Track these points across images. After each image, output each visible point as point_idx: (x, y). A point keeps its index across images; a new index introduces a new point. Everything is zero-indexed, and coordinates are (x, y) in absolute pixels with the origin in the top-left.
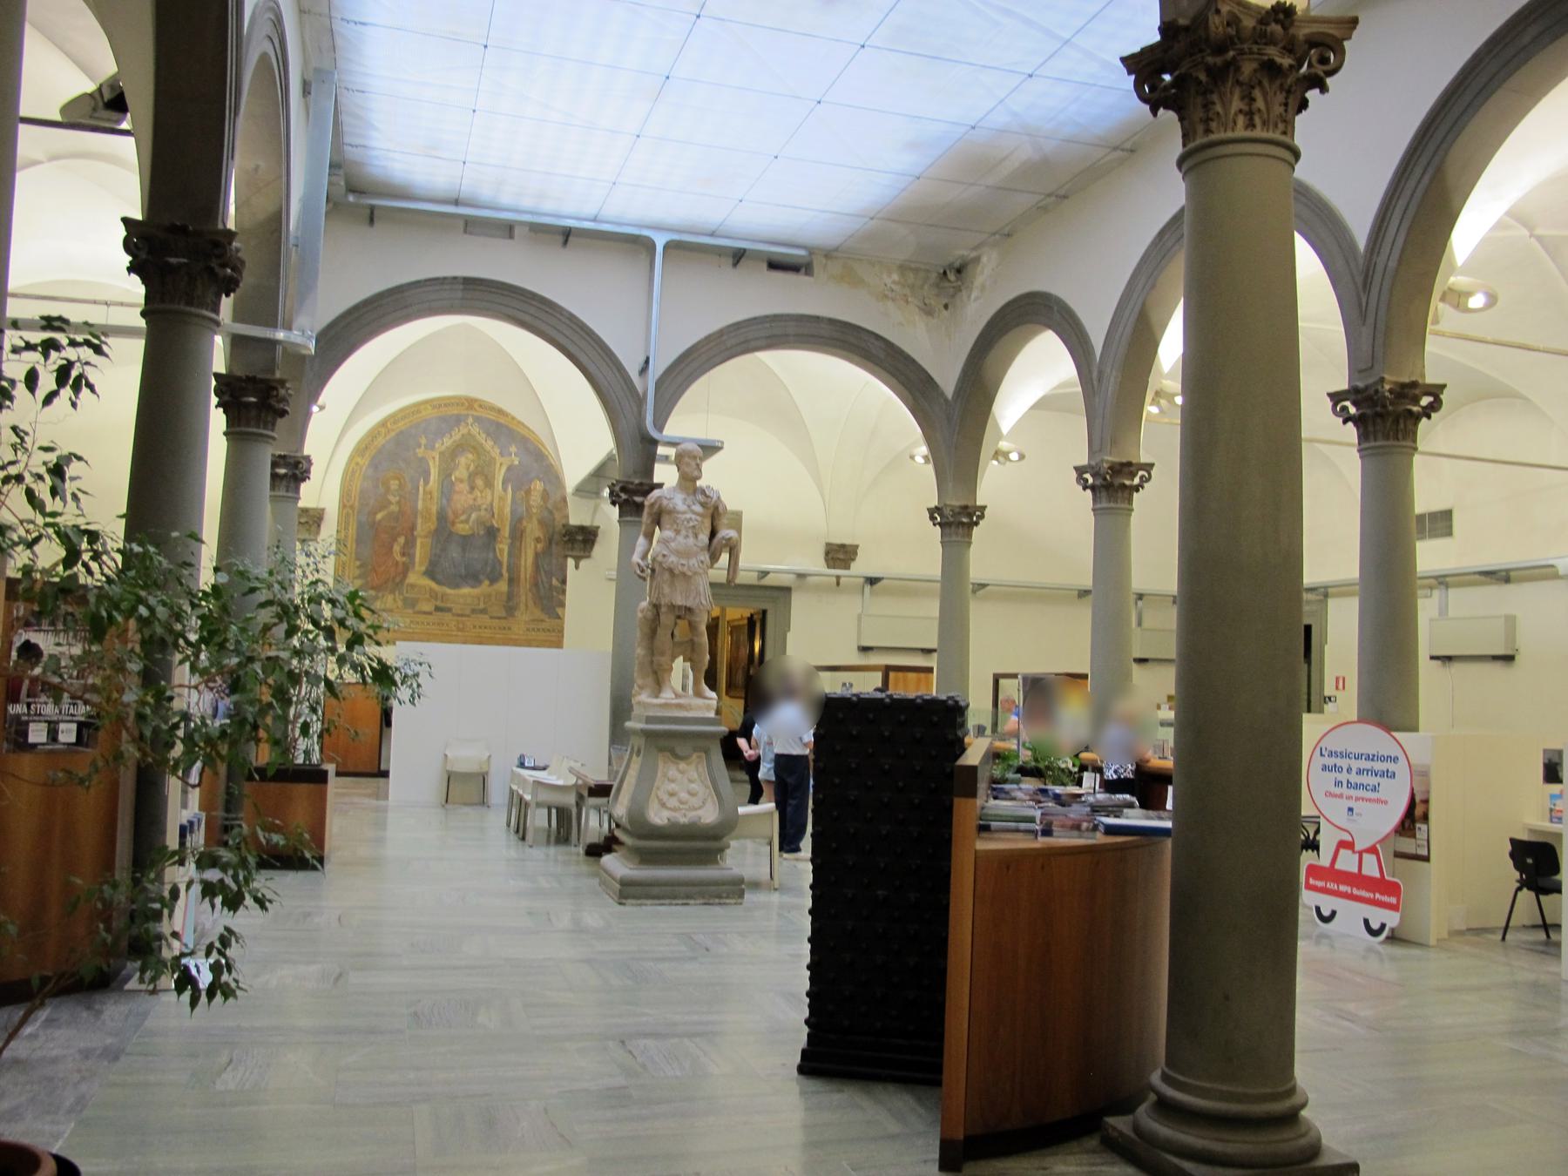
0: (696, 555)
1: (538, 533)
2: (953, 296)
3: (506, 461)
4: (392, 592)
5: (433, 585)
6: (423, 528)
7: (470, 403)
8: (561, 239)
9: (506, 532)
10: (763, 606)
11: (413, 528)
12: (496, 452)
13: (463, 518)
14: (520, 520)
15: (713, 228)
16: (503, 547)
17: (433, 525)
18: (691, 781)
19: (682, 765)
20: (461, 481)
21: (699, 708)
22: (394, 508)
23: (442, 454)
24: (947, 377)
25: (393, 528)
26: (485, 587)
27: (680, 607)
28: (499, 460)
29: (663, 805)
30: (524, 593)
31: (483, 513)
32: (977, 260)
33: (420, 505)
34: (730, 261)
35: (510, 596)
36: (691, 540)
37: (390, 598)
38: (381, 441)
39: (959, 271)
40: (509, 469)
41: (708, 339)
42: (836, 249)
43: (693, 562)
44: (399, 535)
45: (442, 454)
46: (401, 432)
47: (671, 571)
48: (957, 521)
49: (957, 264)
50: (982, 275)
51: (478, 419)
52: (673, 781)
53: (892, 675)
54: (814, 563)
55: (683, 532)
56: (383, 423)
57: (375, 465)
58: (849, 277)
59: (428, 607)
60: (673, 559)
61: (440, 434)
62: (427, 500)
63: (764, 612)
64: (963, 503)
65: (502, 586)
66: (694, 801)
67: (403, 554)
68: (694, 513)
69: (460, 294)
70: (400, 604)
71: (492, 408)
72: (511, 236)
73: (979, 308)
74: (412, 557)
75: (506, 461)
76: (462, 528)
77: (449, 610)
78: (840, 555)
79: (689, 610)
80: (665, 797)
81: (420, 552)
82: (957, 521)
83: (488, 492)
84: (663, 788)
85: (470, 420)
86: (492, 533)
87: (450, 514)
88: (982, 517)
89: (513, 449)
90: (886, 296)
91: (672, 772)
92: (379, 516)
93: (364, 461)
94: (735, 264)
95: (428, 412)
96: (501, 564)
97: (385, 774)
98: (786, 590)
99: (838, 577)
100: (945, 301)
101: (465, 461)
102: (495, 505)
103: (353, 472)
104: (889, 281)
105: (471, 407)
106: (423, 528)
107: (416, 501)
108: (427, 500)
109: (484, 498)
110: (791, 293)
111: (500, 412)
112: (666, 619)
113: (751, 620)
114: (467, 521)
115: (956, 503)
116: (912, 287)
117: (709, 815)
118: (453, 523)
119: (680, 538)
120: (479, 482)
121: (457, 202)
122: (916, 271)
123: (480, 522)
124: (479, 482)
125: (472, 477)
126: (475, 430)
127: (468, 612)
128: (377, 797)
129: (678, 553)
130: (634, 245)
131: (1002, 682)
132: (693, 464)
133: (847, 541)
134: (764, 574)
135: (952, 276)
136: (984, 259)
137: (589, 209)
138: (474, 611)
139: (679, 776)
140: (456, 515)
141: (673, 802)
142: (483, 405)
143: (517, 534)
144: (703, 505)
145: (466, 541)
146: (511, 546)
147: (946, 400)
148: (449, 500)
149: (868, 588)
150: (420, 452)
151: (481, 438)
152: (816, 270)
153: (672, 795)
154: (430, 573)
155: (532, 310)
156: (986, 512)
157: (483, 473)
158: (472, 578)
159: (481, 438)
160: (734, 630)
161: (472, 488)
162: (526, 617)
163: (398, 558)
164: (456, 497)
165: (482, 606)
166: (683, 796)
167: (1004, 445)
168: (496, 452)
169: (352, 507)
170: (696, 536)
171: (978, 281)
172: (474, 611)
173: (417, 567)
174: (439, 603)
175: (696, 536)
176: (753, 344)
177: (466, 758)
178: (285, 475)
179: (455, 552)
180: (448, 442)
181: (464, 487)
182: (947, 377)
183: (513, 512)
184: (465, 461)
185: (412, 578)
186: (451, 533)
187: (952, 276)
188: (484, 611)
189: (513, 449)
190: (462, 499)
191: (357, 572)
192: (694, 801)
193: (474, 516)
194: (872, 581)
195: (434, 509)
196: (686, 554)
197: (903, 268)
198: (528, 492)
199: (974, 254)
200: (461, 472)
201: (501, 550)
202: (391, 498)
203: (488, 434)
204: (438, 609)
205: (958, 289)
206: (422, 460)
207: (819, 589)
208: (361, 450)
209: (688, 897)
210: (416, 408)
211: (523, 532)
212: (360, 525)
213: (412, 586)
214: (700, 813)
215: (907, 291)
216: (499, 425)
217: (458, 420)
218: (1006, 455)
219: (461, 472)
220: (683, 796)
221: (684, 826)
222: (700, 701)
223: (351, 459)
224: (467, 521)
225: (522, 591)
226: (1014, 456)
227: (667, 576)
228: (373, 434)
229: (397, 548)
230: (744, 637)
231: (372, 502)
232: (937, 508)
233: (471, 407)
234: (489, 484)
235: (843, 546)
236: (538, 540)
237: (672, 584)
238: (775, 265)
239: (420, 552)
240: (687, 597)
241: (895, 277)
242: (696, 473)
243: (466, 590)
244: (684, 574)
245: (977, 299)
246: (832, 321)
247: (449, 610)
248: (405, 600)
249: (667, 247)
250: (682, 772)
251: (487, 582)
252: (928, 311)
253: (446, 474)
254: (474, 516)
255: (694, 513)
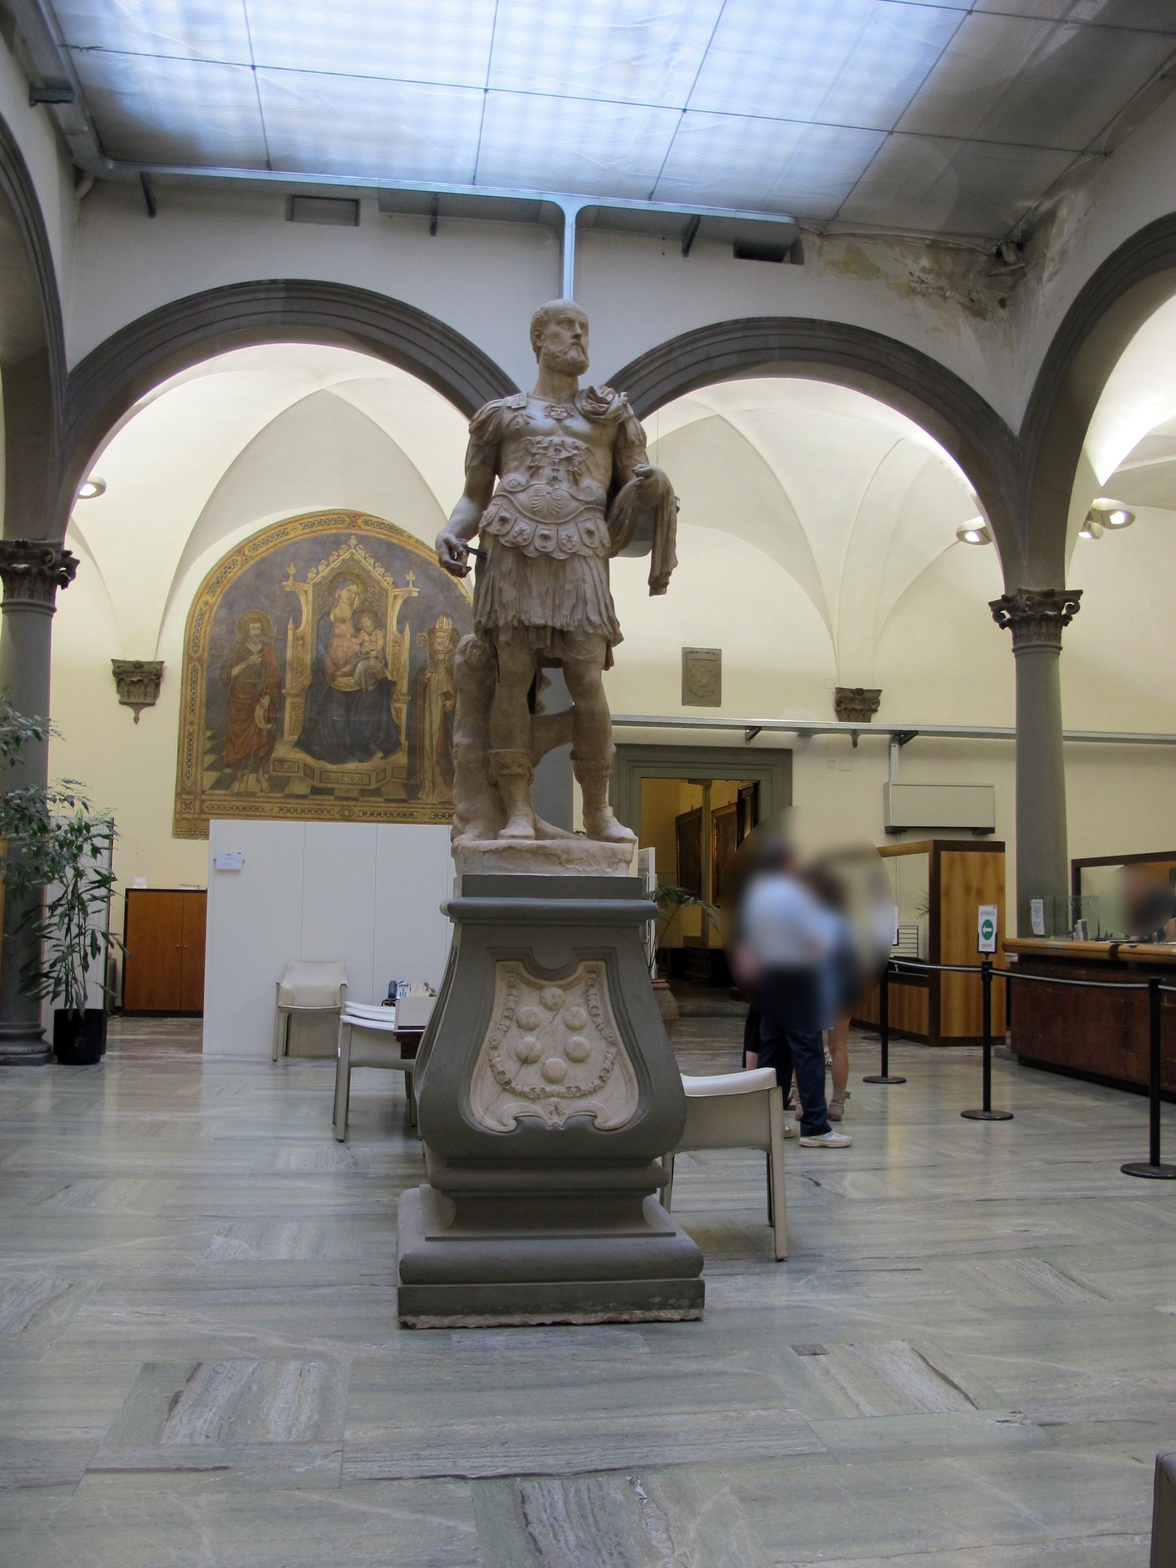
0: (574, 518)
1: (446, 687)
2: (1012, 288)
3: (402, 593)
4: (255, 770)
5: (309, 759)
6: (294, 683)
7: (353, 518)
8: (426, 221)
9: (404, 686)
10: (756, 776)
11: (280, 685)
12: (387, 581)
13: (346, 669)
14: (422, 670)
15: (650, 184)
16: (401, 708)
17: (306, 680)
18: (573, 1029)
19: (552, 992)
20: (343, 621)
21: (591, 858)
22: (255, 659)
23: (315, 585)
24: (1011, 400)
25: (255, 685)
26: (377, 760)
27: (540, 629)
28: (393, 592)
29: (506, 1086)
30: (429, 765)
31: (372, 662)
32: (1052, 214)
33: (289, 654)
34: (680, 245)
35: (412, 770)
36: (564, 488)
37: (252, 778)
38: (236, 573)
39: (1020, 247)
40: (405, 604)
41: (652, 356)
42: (835, 217)
43: (570, 532)
44: (261, 695)
45: (315, 585)
46: (263, 560)
47: (517, 550)
48: (1036, 614)
49: (1017, 234)
50: (1063, 235)
51: (362, 540)
52: (530, 1029)
53: (944, 855)
54: (823, 715)
55: (547, 472)
56: (239, 550)
57: (229, 603)
58: (858, 266)
59: (301, 788)
60: (523, 525)
61: (314, 561)
62: (297, 649)
63: (756, 785)
64: (1045, 588)
65: (401, 758)
66: (582, 1076)
67: (268, 720)
68: (574, 434)
69: (278, 306)
70: (265, 785)
71: (382, 524)
72: (356, 221)
73: (1054, 292)
74: (279, 722)
75: (402, 593)
76: (345, 683)
77: (329, 792)
78: (856, 703)
79: (561, 635)
80: (510, 1067)
81: (290, 717)
82: (1036, 614)
83: (379, 634)
84: (504, 1045)
85: (353, 542)
86: (385, 687)
87: (329, 664)
88: (1075, 609)
89: (410, 577)
90: (913, 291)
91: (529, 1006)
92: (236, 671)
93: (214, 600)
94: (686, 251)
95: (297, 533)
96: (397, 728)
97: (200, 1014)
98: (784, 756)
99: (855, 733)
100: (1001, 295)
101: (347, 595)
102: (389, 651)
103: (202, 614)
104: (915, 268)
105: (353, 524)
106: (294, 683)
107: (284, 649)
108: (297, 649)
109: (373, 642)
110: (771, 278)
111: (392, 528)
112: (514, 662)
113: (741, 803)
114: (351, 674)
115: (1035, 587)
116: (950, 276)
117: (616, 1107)
118: (333, 677)
119: (540, 484)
120: (367, 622)
121: (269, 166)
122: (957, 251)
123: (369, 674)
124: (367, 622)
125: (357, 614)
126: (360, 554)
127: (355, 794)
128: (183, 1046)
129: (534, 514)
130: (532, 221)
131: (1085, 871)
132: (567, 335)
133: (865, 686)
134: (755, 730)
135: (1010, 256)
136: (1063, 212)
137: (463, 162)
138: (363, 793)
139: (544, 1015)
140: (338, 667)
141: (528, 1078)
142: (369, 521)
143: (419, 689)
144: (588, 416)
145: (351, 699)
146: (412, 704)
147: (1010, 434)
148: (327, 647)
149: (895, 749)
150: (288, 585)
151: (368, 564)
152: (806, 255)
153: (525, 1061)
154: (303, 744)
155: (389, 324)
156: (1082, 601)
157: (370, 610)
158: (362, 750)
159: (368, 564)
160: (720, 819)
161: (358, 630)
162: (433, 799)
163: (262, 725)
164: (336, 642)
165: (374, 786)
166: (556, 1062)
167: (1102, 503)
168: (387, 581)
169: (200, 659)
170: (575, 479)
171: (1056, 246)
172: (363, 793)
173: (287, 737)
174: (317, 784)
175: (575, 479)
176: (718, 364)
177: (311, 986)
178: (26, 572)
179: (336, 715)
180: (324, 570)
181: (346, 629)
182: (1011, 400)
183: (412, 660)
184: (347, 595)
185: (283, 750)
186: (331, 691)
187: (1010, 256)
188: (376, 792)
189: (410, 577)
190: (345, 644)
191: (208, 745)
192: (582, 1076)
193: (361, 666)
194: (902, 737)
195: (308, 658)
196: (554, 516)
197: (934, 247)
198: (432, 632)
199: (1047, 205)
200: (342, 610)
201: (398, 710)
202: (251, 646)
203: (377, 559)
204: (315, 791)
205: (1019, 274)
206: (292, 596)
207: (829, 752)
208: (210, 585)
209: (569, 1307)
210: (282, 528)
211: (426, 686)
212: (211, 684)
213: (282, 761)
214: (592, 1103)
215: (943, 282)
216: (390, 545)
217: (337, 542)
218: (1103, 517)
219: (342, 610)
220: (556, 1062)
221: (555, 1133)
222: (593, 845)
223: (199, 596)
224: (351, 674)
225: (427, 764)
226: (1118, 518)
227: (509, 563)
228: (225, 565)
229: (259, 712)
230: (733, 829)
231: (226, 652)
232: (1005, 598)
233: (353, 524)
234: (380, 623)
235: (860, 692)
236: (446, 696)
237: (521, 583)
238: (746, 251)
239: (290, 717)
240: (556, 608)
241: (925, 262)
242: (573, 354)
243: (352, 766)
244: (547, 557)
245: (1050, 279)
246: (835, 327)
247: (329, 792)
248: (271, 780)
249: (581, 216)
250: (552, 1008)
251: (380, 754)
252: (976, 310)
253: (322, 613)
254: (361, 666)
255: (574, 434)
